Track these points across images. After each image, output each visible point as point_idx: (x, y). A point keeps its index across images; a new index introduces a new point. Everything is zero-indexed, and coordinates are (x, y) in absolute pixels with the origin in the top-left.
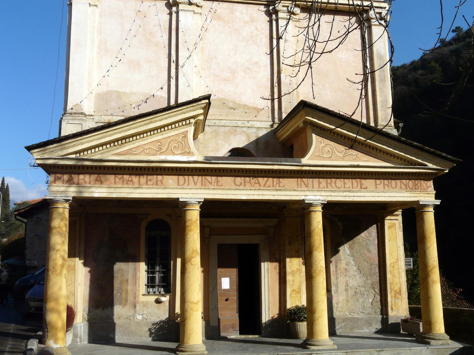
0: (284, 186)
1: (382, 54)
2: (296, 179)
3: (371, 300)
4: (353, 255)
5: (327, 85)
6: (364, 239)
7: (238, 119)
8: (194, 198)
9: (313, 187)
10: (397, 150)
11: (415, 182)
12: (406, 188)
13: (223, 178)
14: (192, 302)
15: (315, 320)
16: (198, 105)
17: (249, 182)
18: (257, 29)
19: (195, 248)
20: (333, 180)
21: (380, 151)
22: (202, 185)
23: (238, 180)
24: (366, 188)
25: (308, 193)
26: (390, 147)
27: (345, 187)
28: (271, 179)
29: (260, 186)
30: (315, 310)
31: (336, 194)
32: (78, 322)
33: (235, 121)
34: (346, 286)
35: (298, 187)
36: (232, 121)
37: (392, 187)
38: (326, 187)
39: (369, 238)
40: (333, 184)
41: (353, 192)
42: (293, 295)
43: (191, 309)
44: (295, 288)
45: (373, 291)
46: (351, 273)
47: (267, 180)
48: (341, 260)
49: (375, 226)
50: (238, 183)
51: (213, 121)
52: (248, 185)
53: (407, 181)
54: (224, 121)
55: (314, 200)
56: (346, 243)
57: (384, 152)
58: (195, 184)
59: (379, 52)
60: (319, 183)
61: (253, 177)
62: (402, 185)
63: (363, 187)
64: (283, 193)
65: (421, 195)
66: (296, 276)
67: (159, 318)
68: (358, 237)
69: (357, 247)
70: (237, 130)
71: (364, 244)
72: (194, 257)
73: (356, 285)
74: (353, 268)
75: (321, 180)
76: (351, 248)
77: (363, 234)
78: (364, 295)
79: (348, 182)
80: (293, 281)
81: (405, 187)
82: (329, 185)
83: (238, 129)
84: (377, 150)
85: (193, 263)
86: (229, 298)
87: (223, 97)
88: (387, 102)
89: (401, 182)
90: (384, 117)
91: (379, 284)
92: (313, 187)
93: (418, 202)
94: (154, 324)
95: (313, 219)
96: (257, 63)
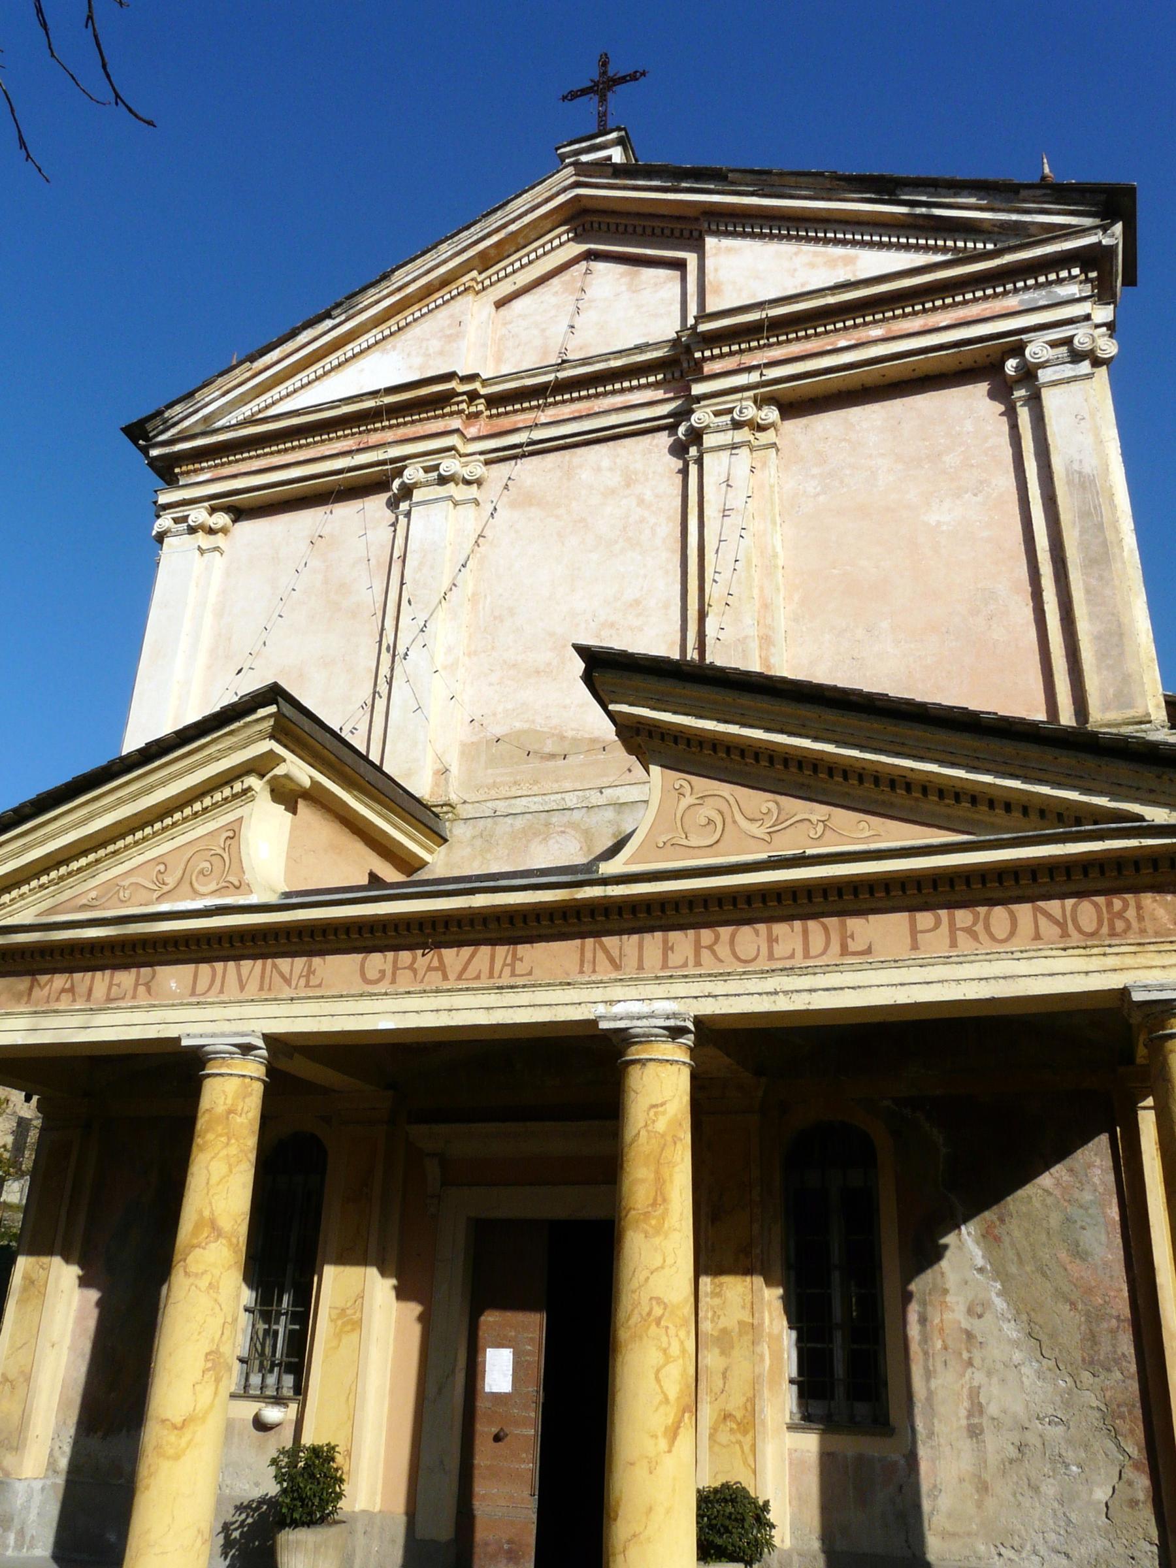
0: (530, 973)
1: (1087, 470)
2: (578, 942)
3: (1101, 1494)
4: (1000, 1273)
5: (885, 625)
6: (1049, 1200)
7: (568, 785)
8: (223, 1035)
9: (641, 967)
10: (988, 772)
11: (1110, 905)
12: (1065, 934)
13: (328, 958)
14: (163, 1421)
15: (614, 1555)
16: (247, 725)
17: (411, 967)
18: (641, 502)
19: (206, 1213)
20: (725, 932)
21: (925, 790)
22: (261, 989)
23: (377, 961)
24: (868, 951)
25: (617, 992)
26: (953, 765)
27: (771, 957)
28: (485, 950)
29: (445, 977)
30: (618, 1504)
31: (732, 986)
32: (29, 1475)
33: (559, 796)
34: (970, 1415)
35: (581, 972)
36: (546, 798)
37: (992, 937)
38: (691, 962)
39: (1076, 1194)
40: (723, 950)
41: (804, 971)
42: (724, 1437)
43: (158, 1447)
44: (730, 1407)
45: (1110, 1445)
46: (996, 1352)
47: (472, 956)
48: (945, 1292)
49: (1103, 1139)
50: (372, 974)
51: (489, 804)
52: (404, 977)
53: (1070, 902)
54: (524, 801)
55: (632, 1018)
56: (965, 1221)
57: (941, 794)
58: (242, 988)
59: (1076, 467)
60: (667, 948)
61: (424, 946)
62: (1043, 922)
63: (853, 946)
64: (524, 997)
65: (1141, 960)
66: (736, 1353)
67: (257, 1484)
68: (1028, 1190)
69: (1017, 1234)
70: (554, 820)
71: (1055, 1220)
72: (199, 1246)
73: (1018, 1408)
74: (1003, 1332)
75: (675, 936)
76: (990, 1238)
77: (1046, 1180)
78: (1067, 1466)
79: (788, 935)
80: (724, 1377)
81: (1057, 930)
82: (705, 954)
83: (555, 818)
84: (908, 787)
85: (193, 1268)
86: (507, 1430)
87: (526, 726)
88: (1121, 635)
89: (1036, 910)
90: (1111, 691)
91: (1138, 1412)
92: (641, 967)
93: (1124, 993)
94: (240, 1508)
95: (632, 1094)
96: (637, 602)
